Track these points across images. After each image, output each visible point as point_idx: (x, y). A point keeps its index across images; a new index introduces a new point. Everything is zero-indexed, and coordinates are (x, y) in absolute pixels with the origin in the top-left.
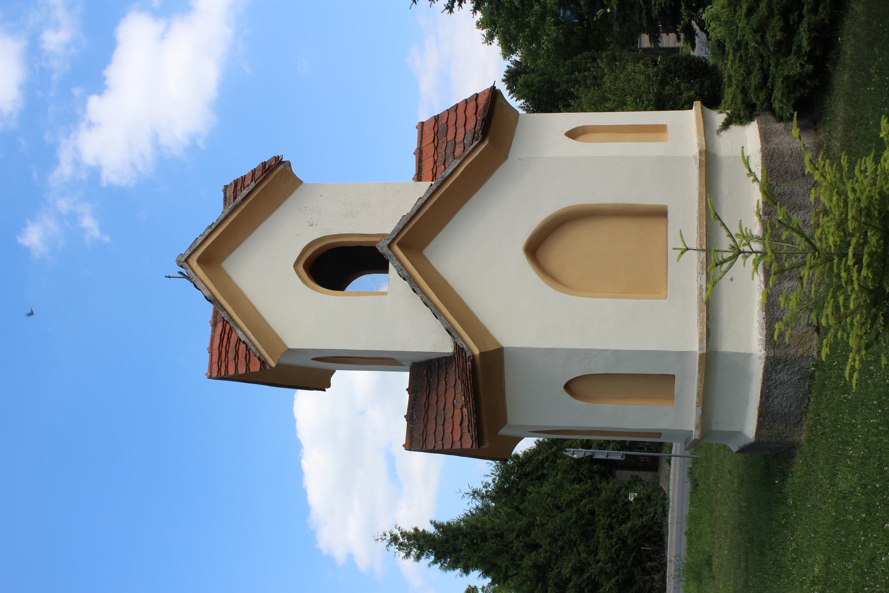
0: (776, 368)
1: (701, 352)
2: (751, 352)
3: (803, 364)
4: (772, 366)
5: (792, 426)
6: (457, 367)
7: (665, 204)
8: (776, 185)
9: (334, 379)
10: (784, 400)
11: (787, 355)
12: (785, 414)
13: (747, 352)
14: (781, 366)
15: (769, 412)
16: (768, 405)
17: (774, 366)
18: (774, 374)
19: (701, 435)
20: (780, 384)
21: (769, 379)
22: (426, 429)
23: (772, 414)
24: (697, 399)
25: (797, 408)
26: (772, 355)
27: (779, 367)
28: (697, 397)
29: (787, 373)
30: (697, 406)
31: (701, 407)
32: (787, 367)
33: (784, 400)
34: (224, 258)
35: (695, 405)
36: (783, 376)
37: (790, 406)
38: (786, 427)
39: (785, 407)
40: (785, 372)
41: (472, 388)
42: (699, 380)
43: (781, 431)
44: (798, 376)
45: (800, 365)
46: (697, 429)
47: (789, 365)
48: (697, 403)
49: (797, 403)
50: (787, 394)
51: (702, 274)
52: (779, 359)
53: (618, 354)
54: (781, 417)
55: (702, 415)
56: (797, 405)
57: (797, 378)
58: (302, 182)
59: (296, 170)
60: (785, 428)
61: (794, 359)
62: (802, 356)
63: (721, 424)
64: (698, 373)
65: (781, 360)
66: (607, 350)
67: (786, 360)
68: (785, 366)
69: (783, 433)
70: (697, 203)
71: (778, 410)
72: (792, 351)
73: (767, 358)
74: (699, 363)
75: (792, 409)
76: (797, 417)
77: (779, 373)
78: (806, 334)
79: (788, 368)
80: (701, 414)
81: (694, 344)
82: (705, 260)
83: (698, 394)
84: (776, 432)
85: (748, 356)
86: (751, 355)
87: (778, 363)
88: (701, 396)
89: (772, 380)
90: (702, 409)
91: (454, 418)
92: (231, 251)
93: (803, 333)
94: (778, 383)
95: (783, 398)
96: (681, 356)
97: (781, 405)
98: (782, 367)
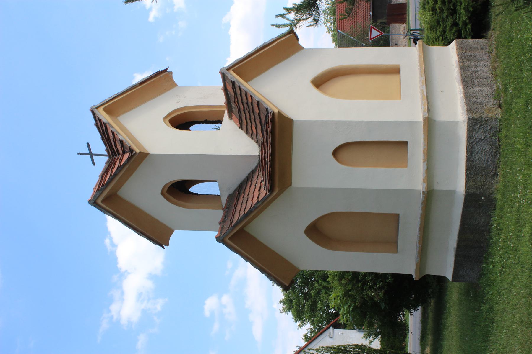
0: (475, 128)
1: (424, 117)
2: (458, 121)
3: (493, 124)
4: (471, 130)
5: (490, 178)
6: (260, 169)
7: (398, 64)
8: (466, 52)
9: (173, 239)
10: (482, 155)
11: (482, 118)
12: (484, 167)
13: (455, 121)
14: (478, 126)
15: (474, 166)
16: (472, 160)
17: (474, 125)
18: (474, 133)
19: (427, 188)
20: (479, 141)
21: (471, 137)
22: (233, 217)
23: (475, 167)
24: (423, 155)
25: (493, 162)
26: (472, 117)
27: (477, 127)
28: (423, 154)
29: (483, 132)
30: (424, 162)
31: (426, 163)
32: (482, 127)
33: (482, 155)
34: (120, 115)
35: (422, 161)
36: (480, 135)
37: (488, 161)
38: (486, 179)
39: (484, 161)
40: (482, 131)
41: (271, 145)
42: (424, 139)
43: (482, 183)
44: (490, 134)
45: (491, 125)
46: (424, 183)
47: (483, 125)
48: (423, 159)
49: (491, 158)
50: (485, 150)
51: (423, 85)
52: (477, 120)
53: (369, 124)
54: (482, 170)
55: (427, 170)
56: (492, 159)
57: (490, 135)
58: (177, 85)
59: (175, 77)
60: (486, 180)
61: (486, 120)
62: (491, 117)
63: (440, 185)
64: (423, 134)
65: (478, 120)
66: (362, 121)
67: (481, 122)
68: (481, 126)
69: (484, 185)
70: (417, 52)
71: (479, 164)
72: (485, 115)
73: (469, 119)
74: (423, 125)
75: (489, 163)
76: (493, 170)
77: (478, 132)
78: (493, 108)
79: (483, 127)
80: (426, 169)
81: (419, 117)
82: (424, 79)
83: (424, 151)
84: (479, 183)
85: (455, 124)
86: (458, 122)
87: (476, 124)
88: (426, 153)
89: (474, 138)
90: (427, 165)
91: (254, 193)
92: (125, 112)
93: (491, 108)
94: (477, 140)
95: (482, 154)
96: (412, 124)
97: (481, 159)
98: (479, 127)
